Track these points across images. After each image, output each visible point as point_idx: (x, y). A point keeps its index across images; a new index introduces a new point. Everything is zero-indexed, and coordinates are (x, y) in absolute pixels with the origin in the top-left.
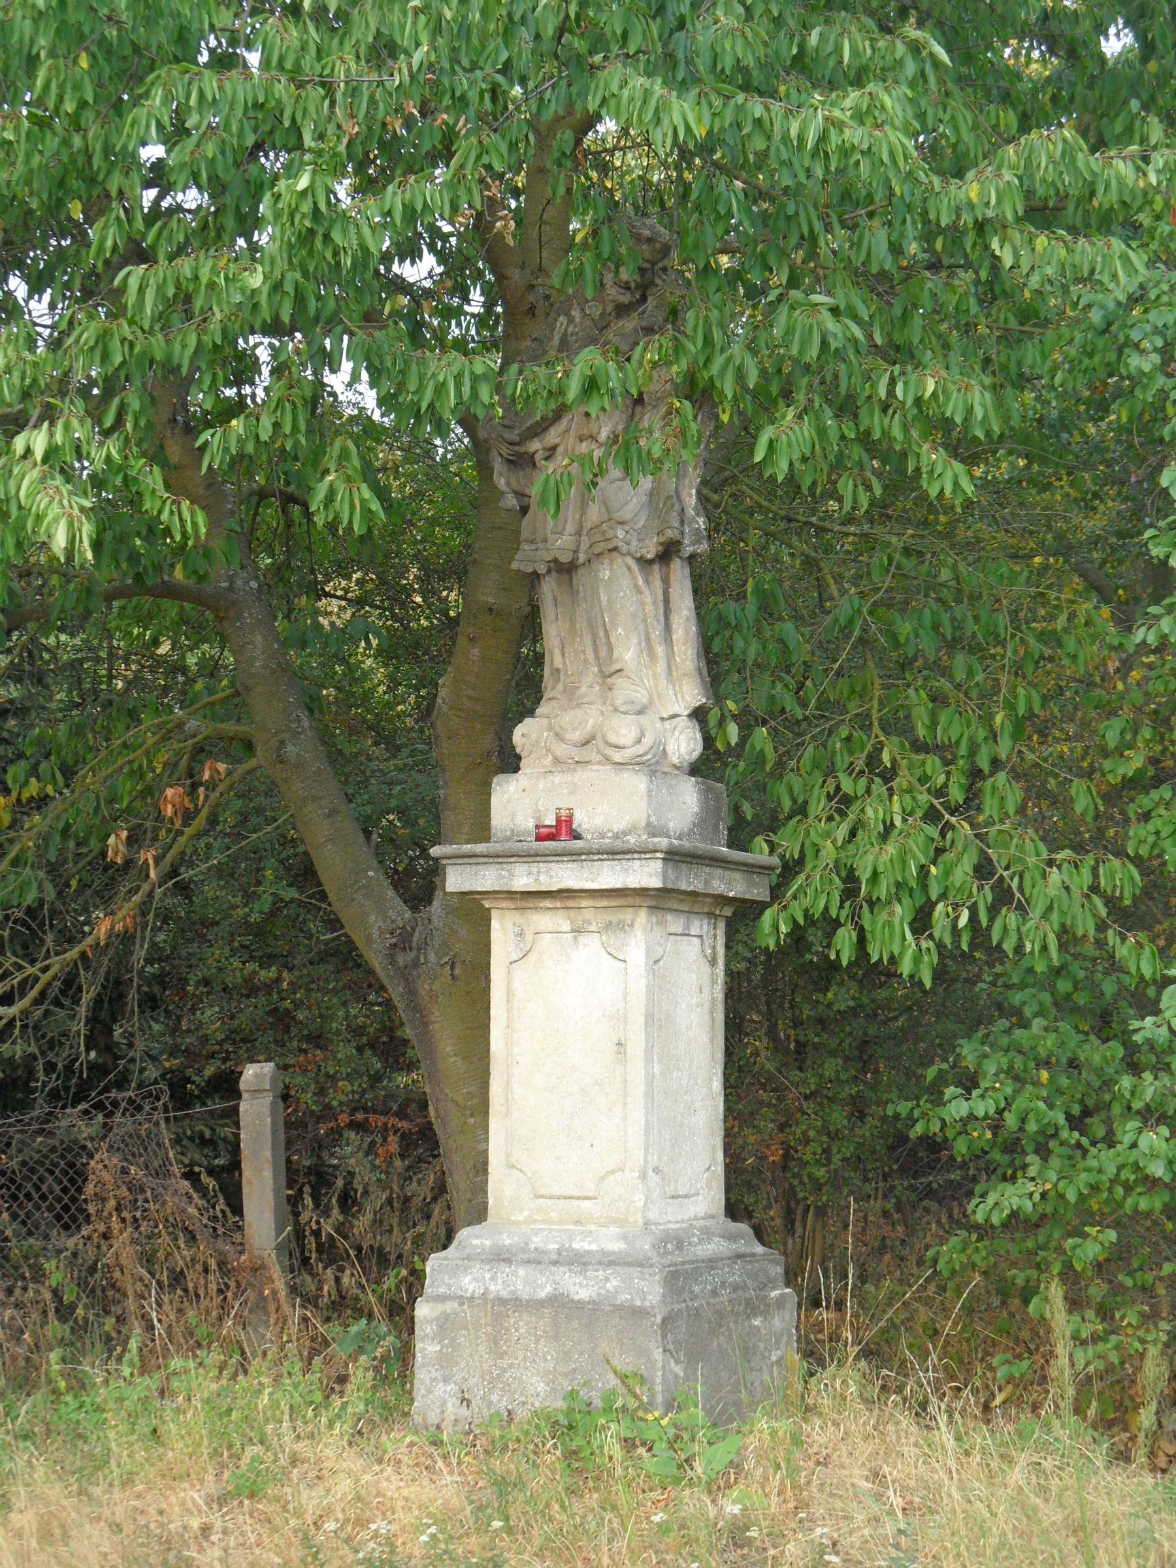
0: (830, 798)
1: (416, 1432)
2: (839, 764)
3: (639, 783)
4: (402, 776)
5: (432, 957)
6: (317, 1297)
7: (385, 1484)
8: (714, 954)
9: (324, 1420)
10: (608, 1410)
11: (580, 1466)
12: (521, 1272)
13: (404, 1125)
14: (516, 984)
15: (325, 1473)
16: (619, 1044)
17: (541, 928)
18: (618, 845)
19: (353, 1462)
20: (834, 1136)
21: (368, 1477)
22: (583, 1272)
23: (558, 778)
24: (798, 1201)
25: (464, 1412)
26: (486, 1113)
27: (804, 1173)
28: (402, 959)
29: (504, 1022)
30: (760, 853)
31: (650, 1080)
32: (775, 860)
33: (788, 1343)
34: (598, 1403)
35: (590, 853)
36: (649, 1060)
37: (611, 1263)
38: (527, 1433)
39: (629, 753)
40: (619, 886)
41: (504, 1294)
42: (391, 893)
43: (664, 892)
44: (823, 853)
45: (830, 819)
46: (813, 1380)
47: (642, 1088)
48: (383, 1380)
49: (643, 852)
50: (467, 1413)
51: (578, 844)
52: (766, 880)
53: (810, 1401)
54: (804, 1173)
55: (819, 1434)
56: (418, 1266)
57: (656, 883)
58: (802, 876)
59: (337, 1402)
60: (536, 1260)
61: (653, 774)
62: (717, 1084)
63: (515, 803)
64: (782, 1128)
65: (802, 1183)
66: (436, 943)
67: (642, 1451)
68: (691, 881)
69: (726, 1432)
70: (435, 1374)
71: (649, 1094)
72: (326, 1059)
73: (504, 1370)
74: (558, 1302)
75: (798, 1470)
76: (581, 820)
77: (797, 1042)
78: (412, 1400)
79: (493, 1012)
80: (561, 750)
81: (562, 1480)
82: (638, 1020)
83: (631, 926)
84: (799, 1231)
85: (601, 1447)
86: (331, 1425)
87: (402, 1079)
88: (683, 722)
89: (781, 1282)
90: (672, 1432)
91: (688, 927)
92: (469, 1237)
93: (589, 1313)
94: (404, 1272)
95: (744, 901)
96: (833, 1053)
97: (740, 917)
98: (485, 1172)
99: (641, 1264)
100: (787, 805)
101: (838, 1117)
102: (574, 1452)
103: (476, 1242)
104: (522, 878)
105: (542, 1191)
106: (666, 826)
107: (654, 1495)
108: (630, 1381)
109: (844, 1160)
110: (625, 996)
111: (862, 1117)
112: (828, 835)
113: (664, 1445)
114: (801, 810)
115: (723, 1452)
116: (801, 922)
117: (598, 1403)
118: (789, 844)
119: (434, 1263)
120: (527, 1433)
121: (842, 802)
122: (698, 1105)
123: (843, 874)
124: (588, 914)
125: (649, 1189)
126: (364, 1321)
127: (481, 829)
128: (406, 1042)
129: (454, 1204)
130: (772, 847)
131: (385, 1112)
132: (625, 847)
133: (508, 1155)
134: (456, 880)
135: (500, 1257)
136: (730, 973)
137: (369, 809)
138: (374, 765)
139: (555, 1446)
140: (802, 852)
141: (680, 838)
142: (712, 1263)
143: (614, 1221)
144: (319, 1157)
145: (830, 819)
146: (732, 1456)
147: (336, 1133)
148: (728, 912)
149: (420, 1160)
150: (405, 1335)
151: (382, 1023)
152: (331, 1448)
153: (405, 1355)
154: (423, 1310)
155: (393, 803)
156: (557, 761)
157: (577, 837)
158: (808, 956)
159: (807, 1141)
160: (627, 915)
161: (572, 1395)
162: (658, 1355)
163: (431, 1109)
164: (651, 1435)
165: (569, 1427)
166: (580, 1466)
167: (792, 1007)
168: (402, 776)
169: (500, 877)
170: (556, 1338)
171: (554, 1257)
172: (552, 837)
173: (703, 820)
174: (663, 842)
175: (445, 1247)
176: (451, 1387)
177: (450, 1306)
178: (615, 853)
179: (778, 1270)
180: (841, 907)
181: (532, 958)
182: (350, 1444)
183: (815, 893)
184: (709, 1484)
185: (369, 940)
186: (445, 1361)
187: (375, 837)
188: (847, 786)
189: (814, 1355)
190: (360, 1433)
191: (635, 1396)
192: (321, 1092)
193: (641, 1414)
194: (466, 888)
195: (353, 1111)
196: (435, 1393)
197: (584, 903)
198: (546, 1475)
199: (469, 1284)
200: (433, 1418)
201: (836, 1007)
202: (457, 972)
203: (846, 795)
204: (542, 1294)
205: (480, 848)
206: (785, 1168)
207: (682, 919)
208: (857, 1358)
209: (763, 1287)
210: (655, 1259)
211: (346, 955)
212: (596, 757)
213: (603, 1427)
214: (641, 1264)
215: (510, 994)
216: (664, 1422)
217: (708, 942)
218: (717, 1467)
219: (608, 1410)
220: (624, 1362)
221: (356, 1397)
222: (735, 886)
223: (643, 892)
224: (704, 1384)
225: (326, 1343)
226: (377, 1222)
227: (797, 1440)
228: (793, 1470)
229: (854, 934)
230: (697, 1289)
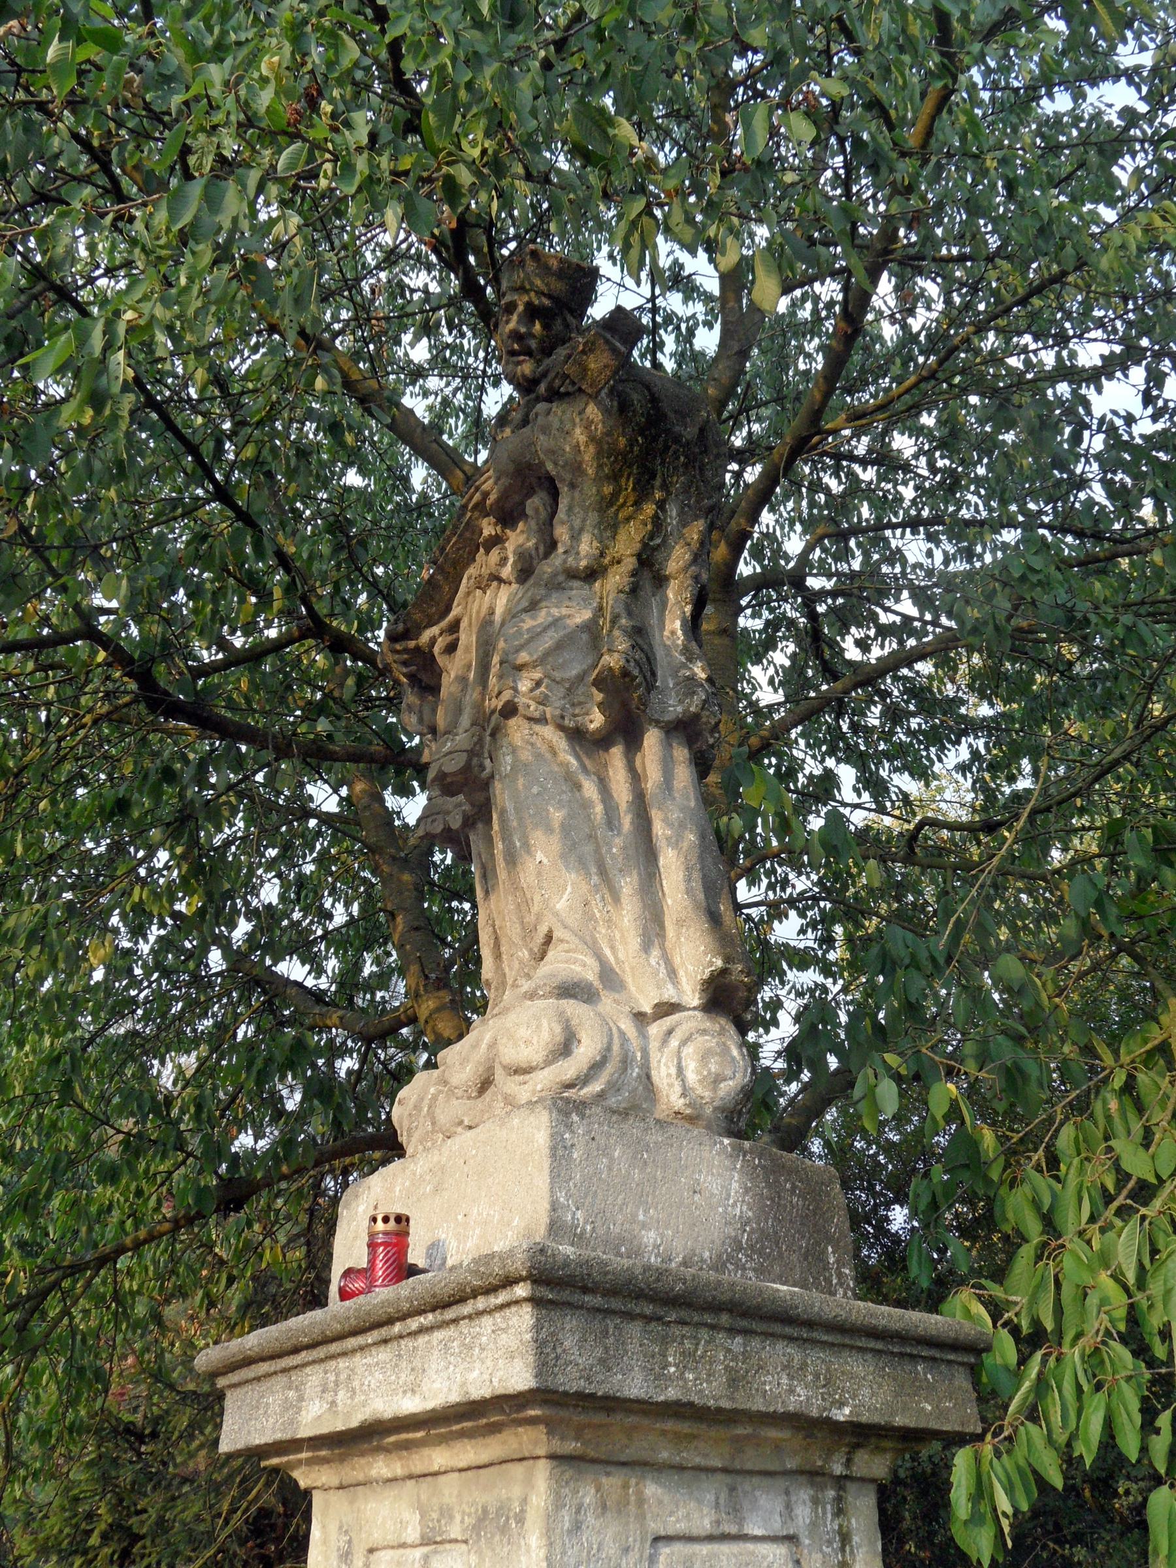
57: (518, 1377)
88: (692, 1020)
148: (875, 1464)
180: (1149, 1426)
197: (439, 1457)
207: (711, 1490)
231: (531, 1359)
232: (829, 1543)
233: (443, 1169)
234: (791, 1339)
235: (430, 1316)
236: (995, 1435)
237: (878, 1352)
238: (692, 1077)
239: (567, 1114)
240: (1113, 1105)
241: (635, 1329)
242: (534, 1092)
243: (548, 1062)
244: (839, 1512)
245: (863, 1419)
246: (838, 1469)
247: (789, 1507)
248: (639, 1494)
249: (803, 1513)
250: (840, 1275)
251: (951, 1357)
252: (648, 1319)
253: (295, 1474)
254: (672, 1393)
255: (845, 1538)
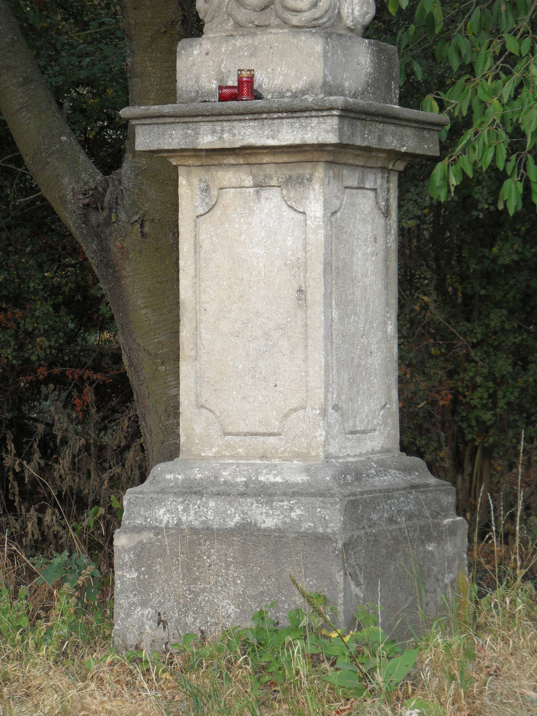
0: (496, 58)
1: (117, 652)
2: (504, 26)
3: (317, 45)
4: (90, 49)
5: (123, 216)
6: (21, 536)
7: (89, 699)
8: (388, 206)
9: (31, 643)
10: (295, 628)
11: (270, 681)
12: (212, 504)
13: (99, 377)
14: (203, 236)
15: (33, 691)
16: (300, 291)
17: (225, 184)
18: (297, 103)
19: (60, 680)
20: (500, 381)
21: (73, 692)
22: (269, 503)
23: (239, 42)
24: (466, 443)
25: (161, 633)
26: (177, 359)
27: (472, 416)
28: (95, 218)
29: (192, 272)
30: (430, 111)
31: (329, 324)
32: (444, 117)
33: (460, 567)
34: (285, 623)
35: (270, 111)
36: (328, 305)
37: (294, 494)
38: (220, 650)
39: (306, 16)
40: (298, 142)
41: (196, 524)
42: (82, 157)
43: (340, 147)
44: (490, 110)
45: (497, 77)
46: (483, 601)
47: (322, 331)
48: (84, 609)
49: (319, 110)
50: (164, 635)
51: (259, 103)
52: (436, 136)
53: (481, 620)
54: (472, 416)
55: (490, 647)
56: (115, 505)
57: (332, 139)
58: (471, 131)
59: (42, 626)
60: (226, 492)
61: (328, 36)
62: (391, 328)
63: (201, 65)
64: (451, 374)
65: (470, 426)
66: (127, 202)
67: (326, 665)
68: (365, 136)
69: (404, 647)
70: (133, 599)
71: (328, 337)
72: (24, 317)
73: (197, 595)
74: (247, 531)
75: (470, 680)
76: (263, 80)
77: (464, 295)
78: (112, 625)
79: (182, 263)
80: (242, 15)
81: (254, 693)
82: (317, 268)
83: (310, 180)
84: (468, 469)
85: (289, 663)
86: (37, 647)
87: (93, 338)
89: (453, 511)
90: (353, 647)
91: (362, 180)
92: (164, 473)
93: (276, 541)
94: (102, 511)
95: (415, 156)
96: (498, 305)
97: (413, 173)
98: (177, 414)
99: (323, 494)
100: (455, 64)
101: (504, 365)
102: (264, 668)
103: (169, 477)
104: (207, 138)
105: (230, 429)
106: (341, 86)
107: (336, 705)
108: (315, 601)
109: (509, 404)
110: (305, 244)
111: (525, 369)
112: (494, 92)
113: (347, 660)
114: (470, 69)
115: (401, 665)
116: (470, 174)
117: (285, 623)
118: (458, 102)
119: (130, 496)
120: (220, 650)
121: (508, 62)
122: (374, 347)
123: (510, 129)
124: (270, 170)
125: (329, 425)
126: (66, 553)
127: (169, 93)
128: (99, 300)
129: (147, 446)
130: (442, 106)
131: (81, 365)
132: (304, 105)
133: (197, 396)
134: (145, 139)
135: (192, 491)
136: (402, 232)
137: (60, 80)
138: (64, 38)
139: (246, 661)
140: (470, 108)
141: (355, 96)
142: (388, 493)
143: (297, 455)
144: (20, 410)
145: (497, 77)
146: (410, 669)
147: (35, 386)
148: (400, 166)
149: (114, 411)
150: (104, 568)
151: (77, 283)
152: (39, 669)
153: (105, 585)
154: (121, 541)
155: (83, 74)
156: (238, 25)
157: (258, 97)
158: (475, 213)
159: (475, 387)
160: (306, 170)
161: (261, 615)
162: (339, 578)
163: (125, 358)
164: (335, 651)
165: (260, 645)
166: (270, 681)
167: (459, 262)
168: (90, 49)
169: (186, 136)
170: (245, 563)
171: (242, 489)
172: (234, 97)
173: (376, 79)
174: (339, 100)
175: (143, 479)
176: (149, 611)
177: (146, 536)
178: (295, 110)
179: (450, 500)
180: (508, 160)
181: (217, 212)
182: (56, 662)
183: (484, 148)
184: (388, 693)
185: (64, 202)
186: (143, 587)
187: (67, 104)
188: (512, 46)
189: (485, 579)
190: (64, 653)
191: (320, 614)
192: (21, 347)
193: (324, 632)
194: (154, 147)
195: (52, 365)
196: (134, 617)
197: (266, 159)
198: (239, 689)
199: (163, 515)
200: (132, 640)
201: (501, 261)
202: (146, 229)
203: (511, 54)
204: (232, 524)
205: (167, 109)
206: (454, 412)
208: (525, 578)
209: (436, 515)
210: (336, 490)
211: (41, 218)
212: (275, 21)
213: (290, 643)
214: (323, 494)
215: (197, 246)
216: (347, 639)
217: (382, 195)
218: (396, 680)
219: (295, 628)
220: (308, 584)
221: (60, 622)
222: (408, 142)
223: (321, 147)
224: (383, 604)
225: (32, 575)
226: (74, 466)
227: (470, 654)
228: (467, 681)
229: (520, 186)
230: (375, 517)
231: (337, 134)
232: (385, 191)
233: (256, 47)
234: (394, 124)
235: (285, 114)
236: (449, 159)
237: (415, 127)
238: (356, 13)
239: (327, 39)
240: (503, 8)
241: (359, 123)
242: (300, 20)
243: (309, 10)
244: (388, 182)
245: (409, 151)
246: (390, 167)
247: (376, 179)
248: (342, 173)
249: (379, 181)
250: (395, 92)
251: (435, 128)
252: (362, 119)
253: (171, 160)
254: (366, 144)
255: (389, 190)
